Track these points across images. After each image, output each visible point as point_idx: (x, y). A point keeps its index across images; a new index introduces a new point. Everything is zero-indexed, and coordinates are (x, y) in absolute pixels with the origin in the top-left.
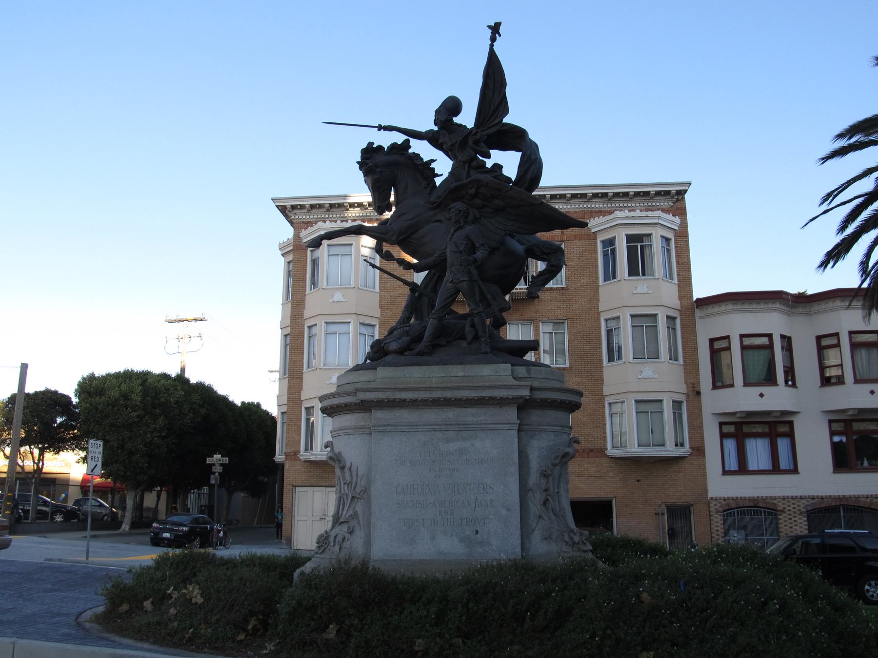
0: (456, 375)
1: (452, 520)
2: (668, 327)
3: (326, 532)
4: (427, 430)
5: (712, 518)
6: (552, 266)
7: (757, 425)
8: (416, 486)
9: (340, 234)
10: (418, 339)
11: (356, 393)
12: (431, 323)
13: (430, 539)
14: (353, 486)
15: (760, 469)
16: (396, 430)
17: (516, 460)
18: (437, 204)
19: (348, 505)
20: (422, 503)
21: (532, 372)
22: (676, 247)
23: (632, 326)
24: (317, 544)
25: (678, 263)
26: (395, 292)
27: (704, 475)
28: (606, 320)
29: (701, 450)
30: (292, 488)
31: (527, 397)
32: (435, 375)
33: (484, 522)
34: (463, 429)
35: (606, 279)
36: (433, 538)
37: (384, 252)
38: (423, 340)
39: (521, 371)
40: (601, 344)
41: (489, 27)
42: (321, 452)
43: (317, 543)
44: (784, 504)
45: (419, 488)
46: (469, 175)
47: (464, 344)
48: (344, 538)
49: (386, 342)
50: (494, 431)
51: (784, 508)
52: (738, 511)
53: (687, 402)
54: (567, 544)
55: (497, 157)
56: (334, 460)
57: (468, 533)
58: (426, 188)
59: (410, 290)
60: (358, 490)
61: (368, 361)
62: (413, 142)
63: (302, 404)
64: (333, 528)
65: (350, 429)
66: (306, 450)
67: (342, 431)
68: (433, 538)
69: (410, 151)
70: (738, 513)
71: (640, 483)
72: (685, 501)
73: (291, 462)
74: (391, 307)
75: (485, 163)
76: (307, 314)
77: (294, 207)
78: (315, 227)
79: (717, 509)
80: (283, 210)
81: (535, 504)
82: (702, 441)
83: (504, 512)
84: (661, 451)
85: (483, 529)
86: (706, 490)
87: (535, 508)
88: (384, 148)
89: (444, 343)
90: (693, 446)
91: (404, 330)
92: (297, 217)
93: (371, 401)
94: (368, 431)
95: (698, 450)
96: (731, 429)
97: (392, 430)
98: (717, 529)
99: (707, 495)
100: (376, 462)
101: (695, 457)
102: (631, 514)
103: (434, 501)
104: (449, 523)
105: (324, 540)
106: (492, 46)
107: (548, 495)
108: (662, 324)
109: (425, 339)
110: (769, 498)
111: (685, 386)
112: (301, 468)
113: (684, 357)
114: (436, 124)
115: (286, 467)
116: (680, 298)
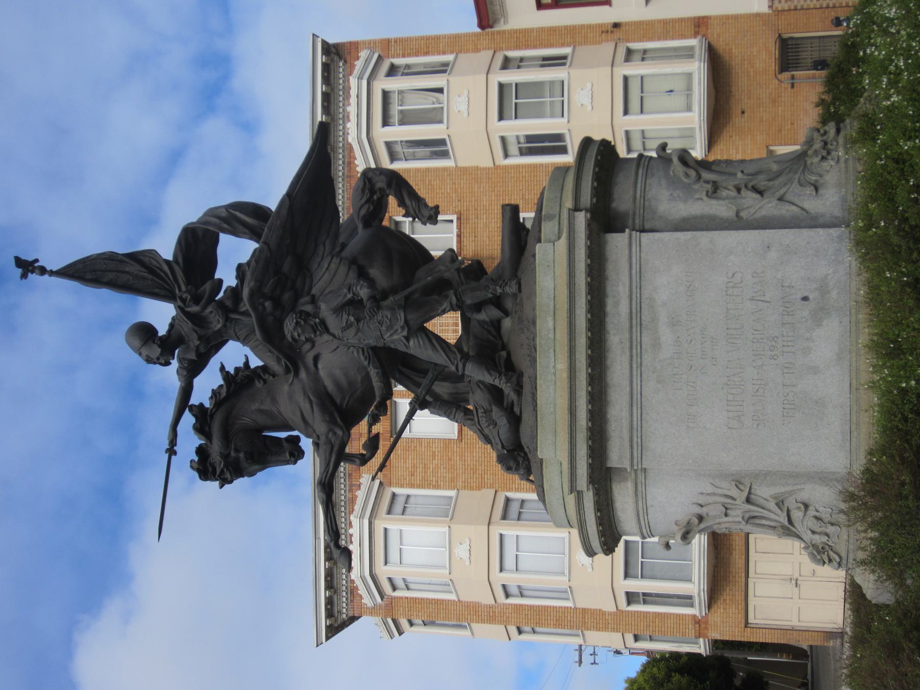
0: (552, 332)
1: (786, 339)
2: (519, 67)
3: (806, 548)
4: (639, 378)
5: (799, 7)
6: (389, 185)
8: (730, 397)
10: (496, 395)
11: (578, 492)
12: (475, 372)
13: (816, 374)
14: (730, 501)
16: (639, 429)
17: (689, 235)
18: (288, 364)
19: (760, 510)
20: (757, 387)
21: (551, 212)
22: (404, 56)
23: (516, 118)
24: (826, 565)
25: (426, 54)
26: (458, 466)
27: (736, 17)
28: (506, 155)
29: (699, 22)
30: (749, 629)
31: (588, 215)
32: (552, 364)
33: (789, 287)
34: (639, 320)
35: (445, 154)
36: (815, 370)
37: (364, 452)
38: (498, 385)
39: (548, 228)
40: (541, 165)
41: (24, 276)
42: (694, 583)
43: (824, 565)
45: (734, 391)
46: (246, 314)
47: (507, 323)
48: (816, 518)
49: (500, 446)
50: (642, 270)
53: (628, 41)
54: (826, 159)
55: (227, 275)
57: (806, 313)
58: (265, 381)
59: (422, 409)
60: (734, 492)
61: (531, 478)
62: (194, 400)
63: (622, 611)
64: (799, 537)
66: (692, 605)
68: (815, 370)
69: (207, 404)
71: (746, 111)
72: (774, 44)
73: (710, 629)
74: (480, 473)
75: (229, 287)
76: (486, 599)
77: (330, 614)
78: (359, 583)
80: (333, 630)
81: (760, 208)
83: (773, 255)
84: (700, 79)
85: (799, 289)
86: (758, 15)
87: (768, 207)
88: (201, 446)
89: (504, 354)
91: (483, 417)
92: (344, 611)
93: (591, 467)
94: (640, 473)
95: (699, 26)
97: (639, 435)
99: (765, 14)
100: (690, 462)
101: (709, 31)
102: (792, 124)
103: (754, 367)
104: (790, 344)
105: (819, 553)
106: (52, 273)
107: (746, 186)
108: (512, 77)
109: (497, 383)
111: (604, 44)
112: (719, 613)
113: (563, 45)
115: (718, 637)
116: (477, 50)
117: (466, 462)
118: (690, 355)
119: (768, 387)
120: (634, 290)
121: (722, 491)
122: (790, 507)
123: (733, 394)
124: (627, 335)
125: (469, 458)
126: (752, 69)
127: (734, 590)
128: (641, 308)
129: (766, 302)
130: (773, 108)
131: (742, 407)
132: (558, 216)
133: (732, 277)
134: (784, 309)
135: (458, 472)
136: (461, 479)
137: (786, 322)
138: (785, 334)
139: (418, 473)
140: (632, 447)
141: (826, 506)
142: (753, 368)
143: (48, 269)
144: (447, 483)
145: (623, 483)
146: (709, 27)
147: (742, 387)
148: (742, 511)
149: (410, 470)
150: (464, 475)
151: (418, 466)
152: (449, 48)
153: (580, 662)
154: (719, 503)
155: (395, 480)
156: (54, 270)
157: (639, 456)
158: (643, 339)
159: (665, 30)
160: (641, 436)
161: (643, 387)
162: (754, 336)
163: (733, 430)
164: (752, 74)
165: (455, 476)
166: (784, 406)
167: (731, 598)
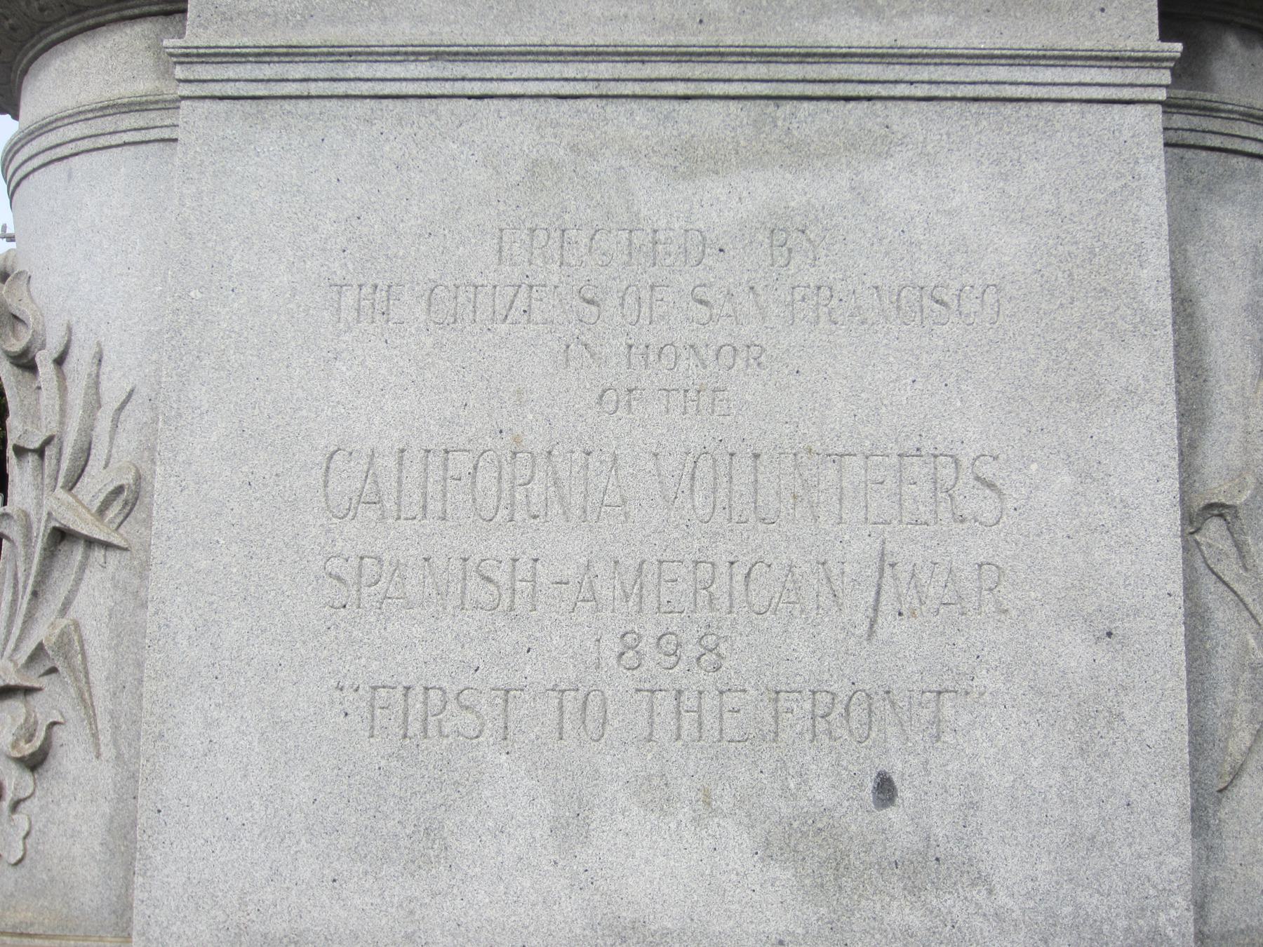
1: (709, 702)
8: (461, 463)
16: (341, 88)
20: (501, 576)
33: (937, 721)
34: (797, 89)
45: (486, 478)
50: (1008, 109)
57: (821, 791)
60: (96, 483)
97: (313, 88)
104: (688, 720)
118: (645, 294)
119: (500, 623)
120: (925, 73)
121: (105, 438)
122: (38, 697)
123: (473, 476)
124: (733, 38)
128: (847, 99)
129: (873, 623)
131: (416, 509)
133: (977, 478)
134: (843, 697)
137: (783, 704)
138: (732, 700)
140: (265, 55)
141: (29, 841)
142: (583, 560)
145: (149, 62)
147: (503, 513)
148: (33, 513)
154: (62, 423)
157: (230, 89)
160: (309, 97)
161: (515, 104)
162: (723, 568)
163: (319, 473)
166: (419, 689)
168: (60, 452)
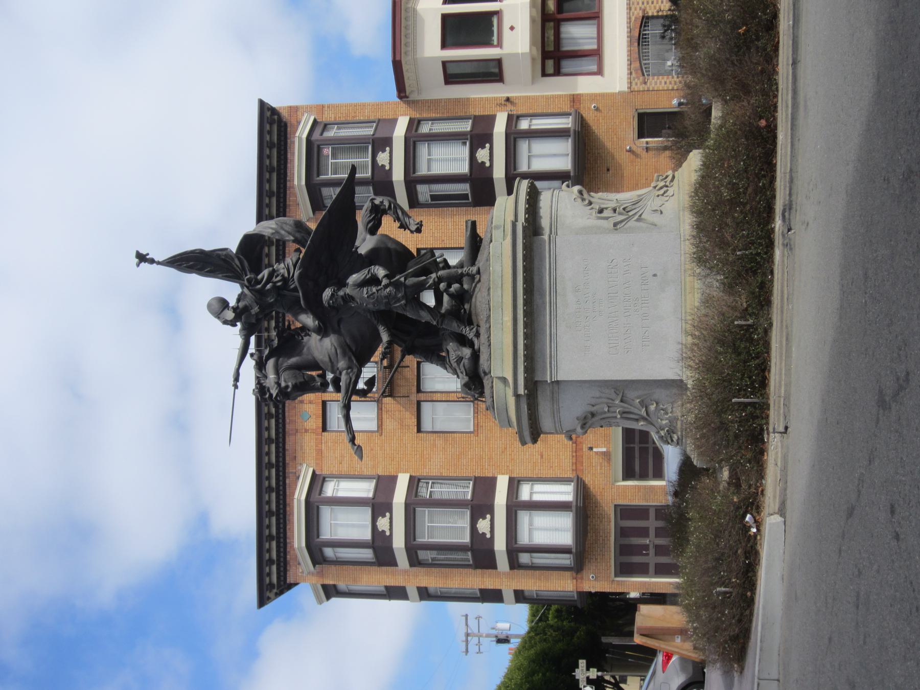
7: (546, 35)
9: (349, 426)
14: (611, 401)
15: (596, 35)
18: (321, 325)
19: (630, 407)
44: (636, 9)
51: (640, 8)
52: (643, 60)
56: (585, 424)
59: (409, 355)
65: (553, 406)
67: (556, 416)
70: (646, 60)
74: (397, 460)
79: (640, 83)
82: (564, 96)
90: (569, 106)
96: (550, 64)
97: (555, 360)
98: (663, 83)
101: (582, 105)
106: (159, 263)
110: (629, 25)
114: (236, 325)
117: (386, 452)
125: (388, 448)
126: (615, 136)
127: (604, 550)
130: (632, 167)
132: (503, 227)
135: (379, 460)
136: (381, 466)
139: (345, 461)
143: (156, 260)
144: (370, 469)
146: (582, 102)
149: (339, 459)
150: (383, 462)
151: (345, 456)
152: (373, 113)
153: (467, 651)
155: (325, 468)
156: (160, 260)
158: (557, 301)
159: (547, 104)
164: (615, 140)
165: (377, 463)
167: (601, 557)
168: (611, 403)
